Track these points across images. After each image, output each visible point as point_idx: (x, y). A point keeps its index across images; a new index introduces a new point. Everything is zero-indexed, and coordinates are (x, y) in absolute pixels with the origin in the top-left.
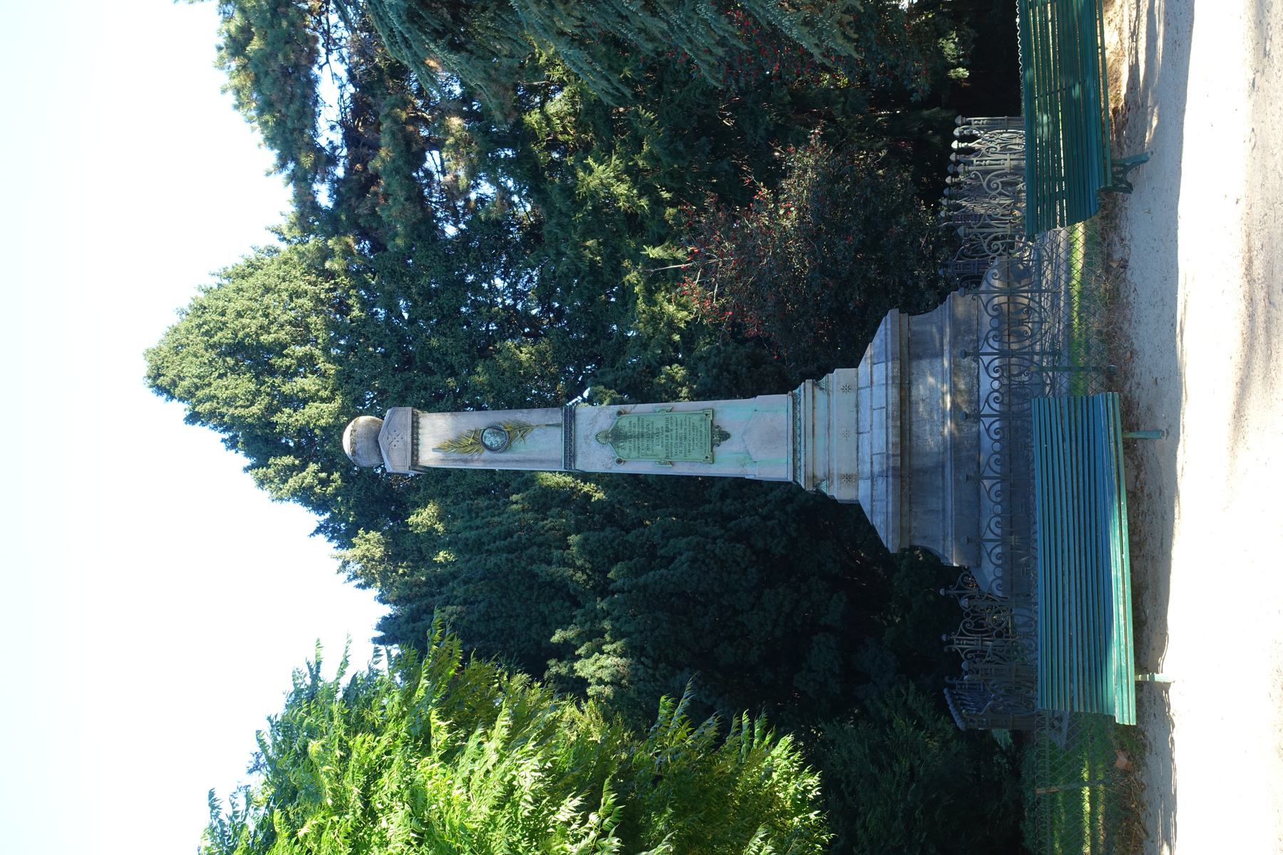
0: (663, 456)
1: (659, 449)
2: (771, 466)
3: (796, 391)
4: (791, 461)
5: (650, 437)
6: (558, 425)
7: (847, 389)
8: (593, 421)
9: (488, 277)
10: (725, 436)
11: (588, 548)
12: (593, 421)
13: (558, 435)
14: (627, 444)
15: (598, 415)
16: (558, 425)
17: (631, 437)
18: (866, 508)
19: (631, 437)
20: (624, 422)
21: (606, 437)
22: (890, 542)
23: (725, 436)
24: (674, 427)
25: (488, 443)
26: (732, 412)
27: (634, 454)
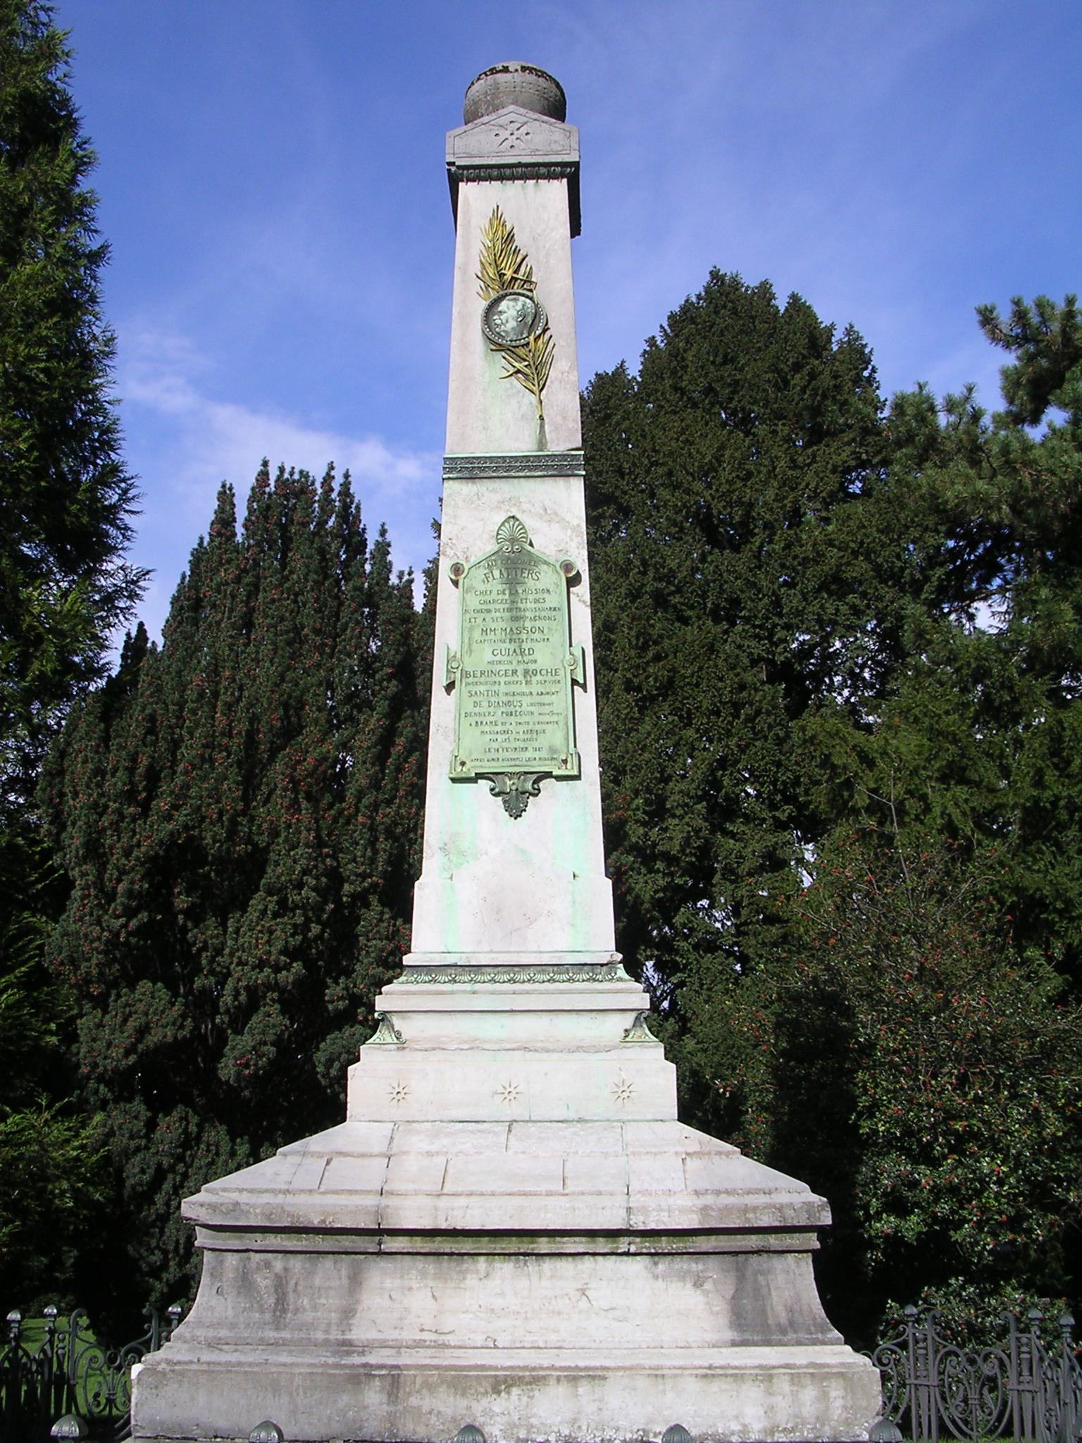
0: (469, 664)
1: (483, 656)
2: (442, 918)
3: (621, 972)
4: (450, 960)
5: (514, 635)
6: (542, 443)
7: (623, 1092)
8: (549, 515)
9: (888, 1130)
10: (515, 804)
11: (28, 233)
12: (549, 515)
13: (523, 445)
14: (496, 585)
15: (564, 524)
16: (542, 443)
17: (514, 593)
18: (318, 1142)
19: (514, 593)
20: (549, 579)
21: (513, 540)
22: (191, 1207)
23: (515, 804)
24: (535, 688)
25: (503, 305)
26: (573, 819)
27: (474, 602)
